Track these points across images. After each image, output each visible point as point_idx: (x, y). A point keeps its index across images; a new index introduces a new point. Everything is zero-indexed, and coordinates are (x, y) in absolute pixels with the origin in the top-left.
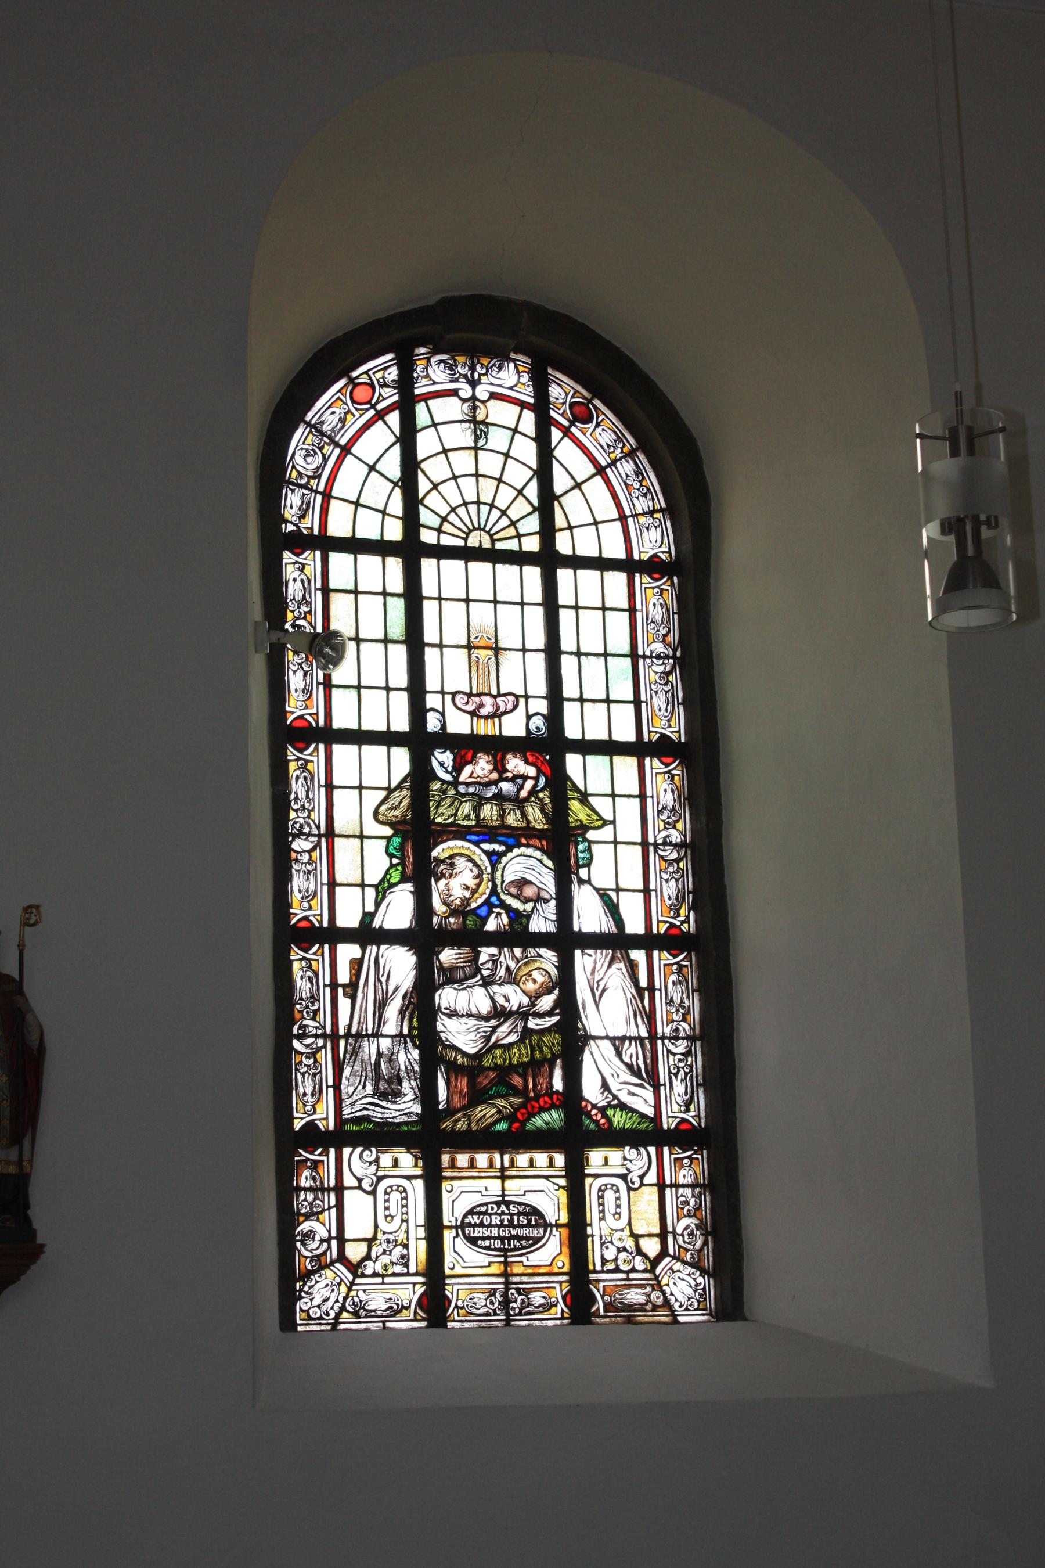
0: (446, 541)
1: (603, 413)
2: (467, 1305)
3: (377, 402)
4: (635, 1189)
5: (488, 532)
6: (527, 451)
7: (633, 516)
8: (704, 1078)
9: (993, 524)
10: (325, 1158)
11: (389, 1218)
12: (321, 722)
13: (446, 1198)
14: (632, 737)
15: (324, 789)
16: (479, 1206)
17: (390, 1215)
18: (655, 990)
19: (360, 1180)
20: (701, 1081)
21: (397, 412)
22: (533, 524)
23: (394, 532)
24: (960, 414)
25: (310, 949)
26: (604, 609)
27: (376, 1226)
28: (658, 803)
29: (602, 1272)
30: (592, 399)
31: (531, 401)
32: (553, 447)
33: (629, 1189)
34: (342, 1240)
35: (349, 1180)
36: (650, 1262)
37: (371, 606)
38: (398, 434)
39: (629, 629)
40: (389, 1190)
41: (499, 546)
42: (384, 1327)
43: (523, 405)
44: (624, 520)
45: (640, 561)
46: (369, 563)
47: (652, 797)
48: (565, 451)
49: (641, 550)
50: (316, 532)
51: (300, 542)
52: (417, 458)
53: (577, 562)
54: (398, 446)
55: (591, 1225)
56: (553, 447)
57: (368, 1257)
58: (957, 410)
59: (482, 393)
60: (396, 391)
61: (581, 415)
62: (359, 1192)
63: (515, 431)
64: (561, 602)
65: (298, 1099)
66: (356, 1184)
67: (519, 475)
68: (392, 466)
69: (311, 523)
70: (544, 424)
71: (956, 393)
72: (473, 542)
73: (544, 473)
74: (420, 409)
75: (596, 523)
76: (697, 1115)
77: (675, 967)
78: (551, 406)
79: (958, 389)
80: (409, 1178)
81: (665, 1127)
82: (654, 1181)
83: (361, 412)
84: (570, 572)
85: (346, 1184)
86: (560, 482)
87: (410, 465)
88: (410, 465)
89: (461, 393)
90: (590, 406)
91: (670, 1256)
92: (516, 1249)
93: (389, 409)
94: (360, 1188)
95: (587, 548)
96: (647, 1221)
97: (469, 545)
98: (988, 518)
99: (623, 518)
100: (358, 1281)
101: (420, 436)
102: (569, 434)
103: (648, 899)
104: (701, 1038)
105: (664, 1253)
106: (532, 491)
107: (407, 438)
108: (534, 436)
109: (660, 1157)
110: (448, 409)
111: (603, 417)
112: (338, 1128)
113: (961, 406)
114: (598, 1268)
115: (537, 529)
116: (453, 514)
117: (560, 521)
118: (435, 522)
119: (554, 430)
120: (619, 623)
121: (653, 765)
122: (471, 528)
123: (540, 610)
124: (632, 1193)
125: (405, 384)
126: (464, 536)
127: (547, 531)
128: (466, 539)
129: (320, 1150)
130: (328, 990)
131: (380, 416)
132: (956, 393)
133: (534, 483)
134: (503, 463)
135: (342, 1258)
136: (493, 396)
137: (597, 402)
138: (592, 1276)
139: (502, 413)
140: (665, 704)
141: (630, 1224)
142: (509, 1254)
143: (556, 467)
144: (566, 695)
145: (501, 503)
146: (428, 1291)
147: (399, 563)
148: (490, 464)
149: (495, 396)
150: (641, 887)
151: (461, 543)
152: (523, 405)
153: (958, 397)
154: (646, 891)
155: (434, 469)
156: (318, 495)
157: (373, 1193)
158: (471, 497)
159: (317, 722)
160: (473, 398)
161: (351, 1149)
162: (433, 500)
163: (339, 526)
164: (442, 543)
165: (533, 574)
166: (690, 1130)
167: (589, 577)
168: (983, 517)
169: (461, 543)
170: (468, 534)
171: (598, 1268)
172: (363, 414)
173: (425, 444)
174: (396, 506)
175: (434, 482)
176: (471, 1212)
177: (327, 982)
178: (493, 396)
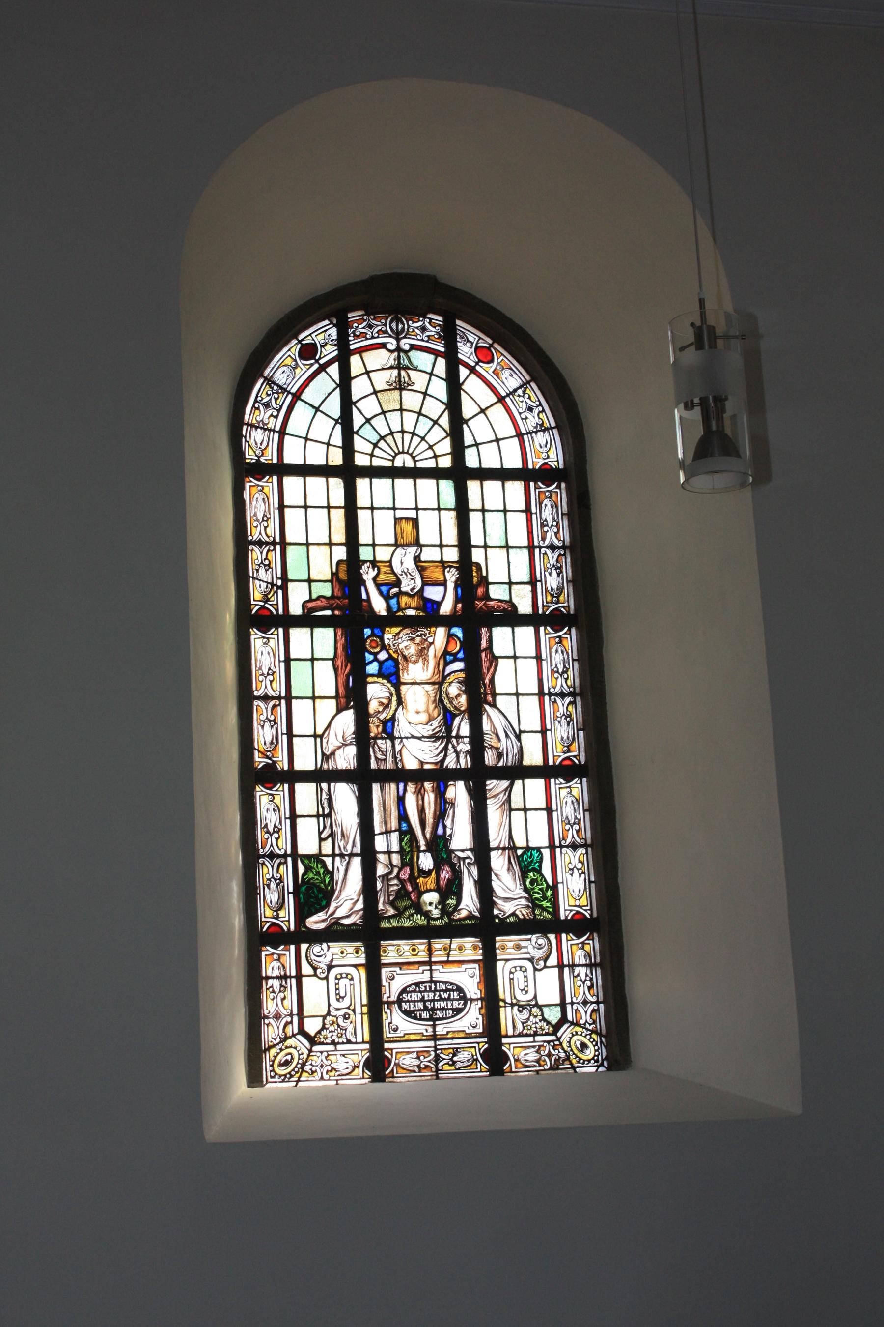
0: (377, 462)
1: (502, 354)
3: (320, 358)
6: (440, 389)
7: (527, 433)
8: (578, 655)
10: (287, 953)
11: (340, 998)
12: (281, 611)
15: (284, 663)
16: (410, 986)
17: (341, 997)
18: (543, 660)
20: (575, 657)
21: (337, 364)
22: (446, 446)
25: (259, 609)
26: (517, 695)
27: (329, 1005)
28: (562, 815)
32: (461, 381)
33: (535, 969)
35: (306, 969)
36: (553, 1026)
37: (318, 517)
39: (542, 754)
41: (420, 465)
42: (337, 1084)
43: (436, 354)
46: (316, 483)
47: (563, 883)
48: (472, 386)
49: (534, 461)
51: (260, 470)
53: (483, 474)
54: (338, 390)
57: (324, 1027)
60: (336, 348)
61: (484, 355)
63: (431, 374)
64: (473, 543)
65: (266, 906)
66: (311, 972)
67: (435, 408)
68: (334, 406)
69: (270, 457)
70: (453, 362)
72: (398, 463)
73: (454, 405)
74: (355, 360)
75: (497, 440)
76: (579, 753)
77: (557, 640)
81: (562, 917)
82: (555, 963)
83: (308, 367)
85: (304, 972)
86: (468, 409)
87: (347, 404)
88: (347, 404)
91: (569, 1022)
94: (315, 975)
95: (491, 461)
100: (315, 1048)
101: (354, 383)
103: (525, 462)
104: (581, 694)
105: (563, 1020)
106: (445, 421)
107: (345, 383)
108: (444, 376)
109: (525, 459)
110: (377, 359)
112: (298, 930)
114: (510, 1033)
115: (449, 450)
117: (468, 440)
118: (369, 448)
119: (461, 368)
124: (537, 972)
125: (342, 343)
126: (391, 458)
127: (458, 450)
128: (393, 461)
129: (282, 947)
130: (288, 821)
131: (323, 368)
135: (302, 1032)
138: (504, 1040)
139: (423, 360)
140: (573, 812)
141: (535, 997)
144: (471, 506)
145: (421, 431)
146: (371, 1057)
147: (340, 483)
148: (411, 400)
152: (436, 354)
154: (538, 658)
155: (369, 406)
157: (326, 978)
160: (399, 349)
161: (308, 945)
163: (293, 455)
164: (374, 464)
165: (447, 487)
167: (493, 486)
169: (389, 464)
170: (394, 457)
173: (359, 388)
175: (397, 850)
176: (404, 991)
177: (288, 815)
178: (413, 347)
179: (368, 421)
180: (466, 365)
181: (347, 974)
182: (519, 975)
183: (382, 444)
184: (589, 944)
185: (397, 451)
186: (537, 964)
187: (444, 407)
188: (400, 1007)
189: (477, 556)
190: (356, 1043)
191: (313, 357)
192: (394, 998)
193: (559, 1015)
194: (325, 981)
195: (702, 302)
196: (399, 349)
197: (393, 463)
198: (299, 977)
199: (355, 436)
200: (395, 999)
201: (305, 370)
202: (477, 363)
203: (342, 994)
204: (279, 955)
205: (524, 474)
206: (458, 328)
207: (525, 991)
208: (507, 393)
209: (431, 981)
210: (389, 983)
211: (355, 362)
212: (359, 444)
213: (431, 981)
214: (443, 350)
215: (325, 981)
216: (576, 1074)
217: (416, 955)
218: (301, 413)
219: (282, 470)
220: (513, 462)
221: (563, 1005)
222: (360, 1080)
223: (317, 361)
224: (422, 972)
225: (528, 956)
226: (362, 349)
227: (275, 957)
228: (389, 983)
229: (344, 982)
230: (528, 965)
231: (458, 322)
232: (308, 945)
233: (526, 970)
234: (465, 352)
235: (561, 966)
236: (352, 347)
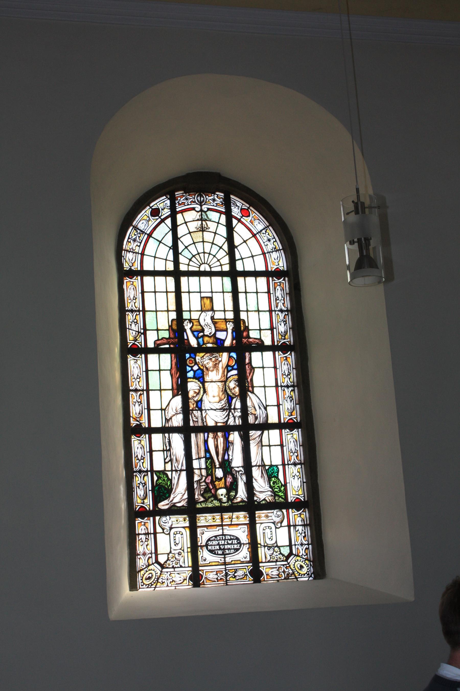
0: (191, 269)
1: (254, 212)
2: (165, 207)
3: (161, 216)
4: (278, 528)
5: (208, 264)
6: (223, 230)
7: (268, 253)
10: (149, 521)
11: (176, 544)
12: (143, 346)
16: (212, 537)
19: (163, 529)
20: (294, 367)
21: (170, 219)
22: (226, 260)
23: (170, 267)
26: (265, 387)
27: (171, 548)
28: (288, 448)
31: (224, 210)
33: (276, 528)
35: (159, 529)
36: (285, 557)
37: (161, 297)
38: (171, 228)
40: (175, 533)
41: (213, 270)
42: (175, 589)
43: (221, 212)
46: (160, 280)
48: (239, 229)
51: (131, 274)
52: (177, 224)
53: (246, 274)
54: (171, 231)
57: (168, 559)
63: (218, 223)
66: (161, 531)
67: (221, 240)
68: (169, 240)
69: (137, 267)
72: (202, 269)
73: (230, 239)
74: (179, 216)
76: (297, 416)
77: (285, 358)
78: (232, 199)
83: (155, 220)
84: (243, 278)
85: (158, 531)
86: (237, 240)
89: (197, 209)
91: (294, 554)
92: (229, 554)
93: (166, 218)
94: (163, 532)
95: (249, 267)
96: (283, 540)
97: (201, 270)
99: (264, 254)
100: (164, 570)
102: (240, 221)
105: (291, 554)
106: (226, 247)
107: (174, 228)
108: (225, 224)
110: (190, 215)
112: (154, 509)
117: (237, 256)
118: (187, 261)
119: (234, 220)
120: (264, 298)
123: (230, 294)
124: (277, 529)
126: (199, 266)
128: (199, 268)
129: (146, 518)
131: (163, 221)
135: (157, 562)
136: (209, 209)
138: (261, 565)
139: (214, 216)
141: (276, 542)
145: (213, 252)
148: (208, 236)
149: (210, 209)
150: (266, 291)
154: (275, 368)
156: (139, 254)
157: (169, 534)
159: (141, 345)
160: (201, 211)
161: (159, 517)
166: (299, 502)
169: (197, 269)
172: (156, 221)
173: (181, 230)
174: (171, 257)
177: (148, 450)
178: (209, 209)
179: (186, 247)
180: (236, 218)
181: (180, 532)
182: (268, 531)
183: (194, 259)
185: (201, 263)
188: (207, 548)
189: (243, 316)
190: (185, 567)
192: (204, 544)
193: (289, 551)
197: (199, 269)
198: (155, 533)
199: (180, 255)
200: (205, 544)
203: (177, 542)
204: (145, 523)
205: (266, 274)
210: (201, 536)
212: (182, 259)
214: (224, 210)
216: (298, 581)
218: (152, 243)
219: (143, 273)
222: (187, 586)
227: (143, 523)
228: (201, 536)
229: (178, 536)
230: (272, 526)
233: (271, 528)
234: (236, 212)
235: (289, 526)
236: (178, 210)
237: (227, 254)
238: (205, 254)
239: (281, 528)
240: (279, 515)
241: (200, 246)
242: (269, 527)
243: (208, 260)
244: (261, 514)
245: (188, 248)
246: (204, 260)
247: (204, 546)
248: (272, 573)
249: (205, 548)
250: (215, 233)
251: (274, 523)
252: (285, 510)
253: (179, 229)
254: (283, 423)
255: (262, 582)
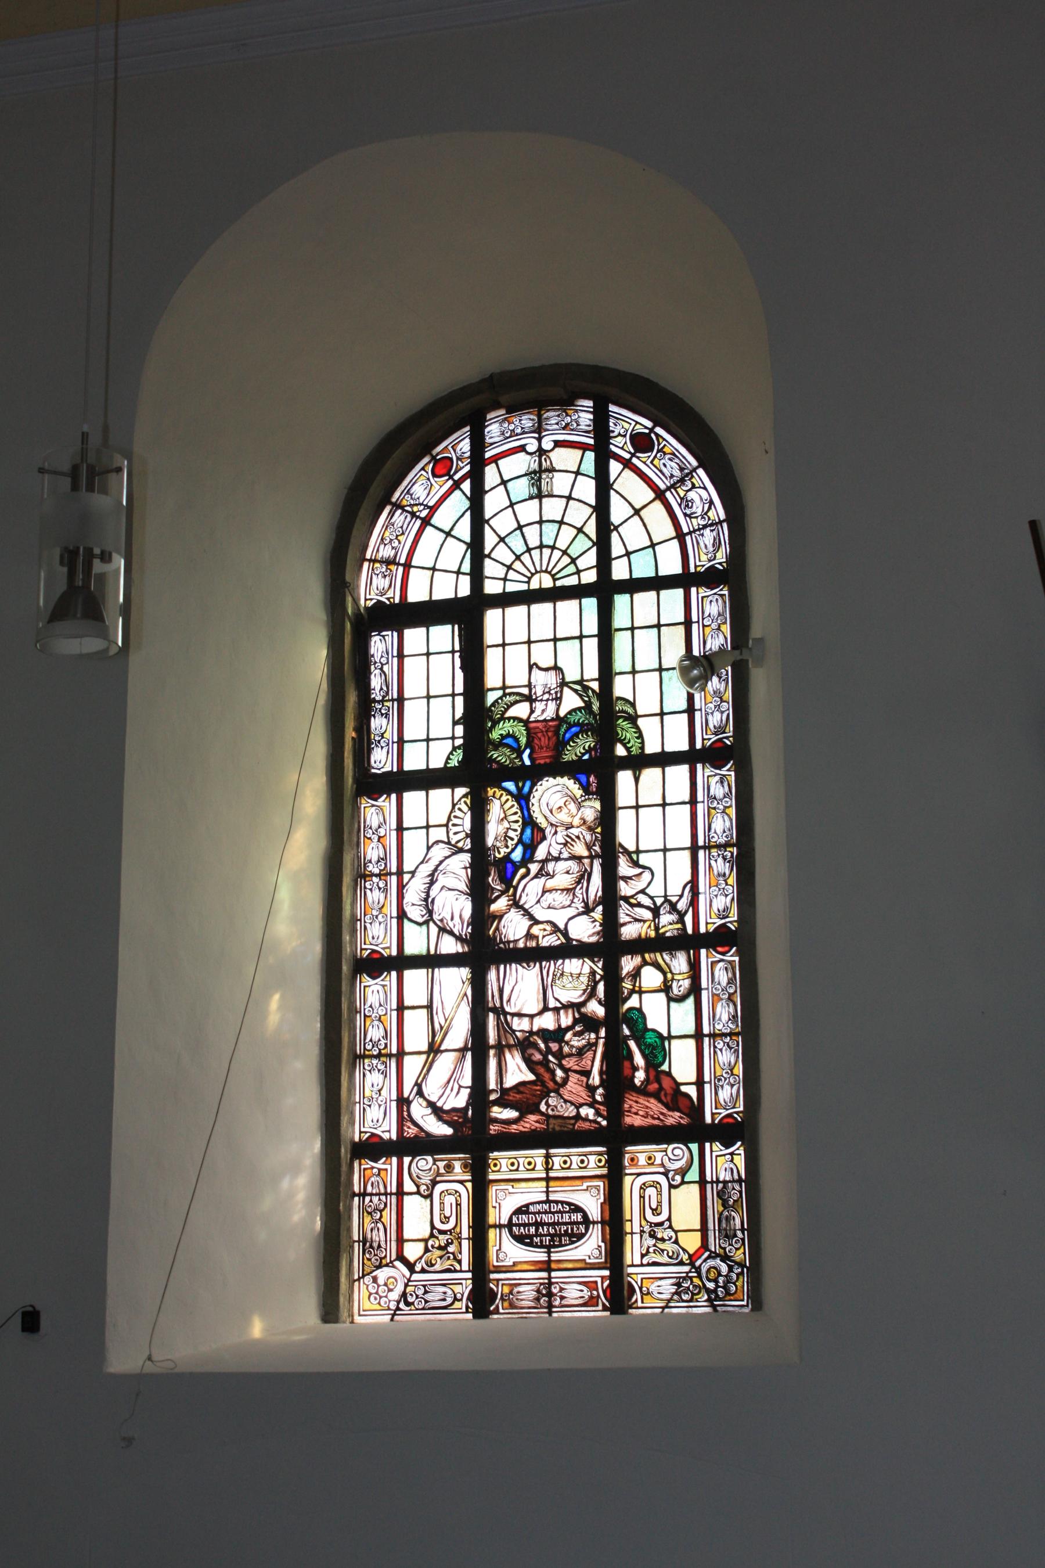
0: (511, 587)
6: (587, 489)
9: (107, 558)
13: (492, 1201)
14: (685, 747)
19: (418, 1186)
22: (591, 558)
24: (84, 453)
27: (433, 1227)
29: (642, 1265)
30: (654, 427)
31: (591, 441)
32: (611, 482)
33: (671, 1187)
34: (401, 1241)
35: (409, 1186)
43: (584, 447)
44: (408, 563)
45: (696, 573)
50: (397, 600)
51: (709, 578)
55: (469, 1227)
56: (611, 482)
58: (82, 448)
59: (547, 444)
62: (417, 1197)
66: (415, 1189)
67: (581, 515)
68: (464, 530)
70: (603, 455)
71: (83, 433)
72: (535, 585)
73: (602, 508)
79: (85, 429)
80: (461, 1182)
86: (618, 511)
87: (479, 522)
88: (479, 522)
90: (438, 457)
93: (463, 479)
94: (418, 1193)
95: (643, 569)
98: (103, 552)
106: (591, 529)
110: (516, 465)
111: (664, 442)
113: (87, 444)
116: (569, 560)
118: (501, 572)
121: (702, 771)
122: (529, 575)
124: (672, 1190)
128: (528, 583)
131: (457, 485)
132: (83, 433)
133: (593, 521)
134: (565, 505)
135: (401, 1258)
137: (659, 430)
141: (669, 1219)
142: (552, 1250)
143: (614, 498)
148: (553, 508)
151: (524, 587)
153: (85, 436)
155: (503, 523)
157: (430, 1196)
158: (548, 541)
160: (541, 452)
161: (410, 1158)
162: (503, 554)
168: (97, 551)
169: (524, 587)
170: (530, 578)
171: (637, 1261)
173: (493, 501)
178: (558, 444)
180: (618, 458)
182: (651, 1191)
183: (566, 560)
184: (740, 1154)
185: (549, 569)
186: (677, 1179)
187: (590, 510)
188: (511, 1232)
189: (621, 687)
190: (461, 1271)
191: (636, 451)
192: (504, 1221)
193: (698, 1244)
194: (428, 1201)
195: (85, 437)
196: (541, 452)
197: (529, 586)
198: (400, 1193)
200: (506, 1223)
201: (442, 485)
202: (451, 477)
203: (448, 1214)
204: (379, 1170)
206: (610, 413)
207: (656, 1212)
208: (667, 486)
209: (548, 1201)
210: (499, 1204)
211: (491, 476)
212: (490, 568)
213: (548, 1201)
214: (591, 441)
215: (428, 1201)
216: (717, 1313)
217: (585, 1168)
218: (431, 537)
219: (685, 580)
220: (670, 565)
221: (704, 1230)
222: (462, 1315)
223: (633, 455)
224: (585, 1188)
225: (662, 1170)
226: (497, 457)
227: (375, 1171)
228: (499, 1204)
230: (662, 1179)
231: (612, 408)
232: (410, 1158)
234: (620, 445)
235: (702, 1182)
237: (594, 544)
238: (533, 552)
239: (682, 1187)
240: (679, 1155)
241: (550, 530)
242: (641, 1188)
243: (558, 565)
244: (637, 1154)
245: (581, 535)
246: (539, 562)
247: (504, 1226)
248: (661, 1290)
249: (505, 1232)
250: (569, 498)
251: (665, 1174)
252: (697, 1144)
253: (488, 499)
254: (703, 934)
255: (630, 1311)
